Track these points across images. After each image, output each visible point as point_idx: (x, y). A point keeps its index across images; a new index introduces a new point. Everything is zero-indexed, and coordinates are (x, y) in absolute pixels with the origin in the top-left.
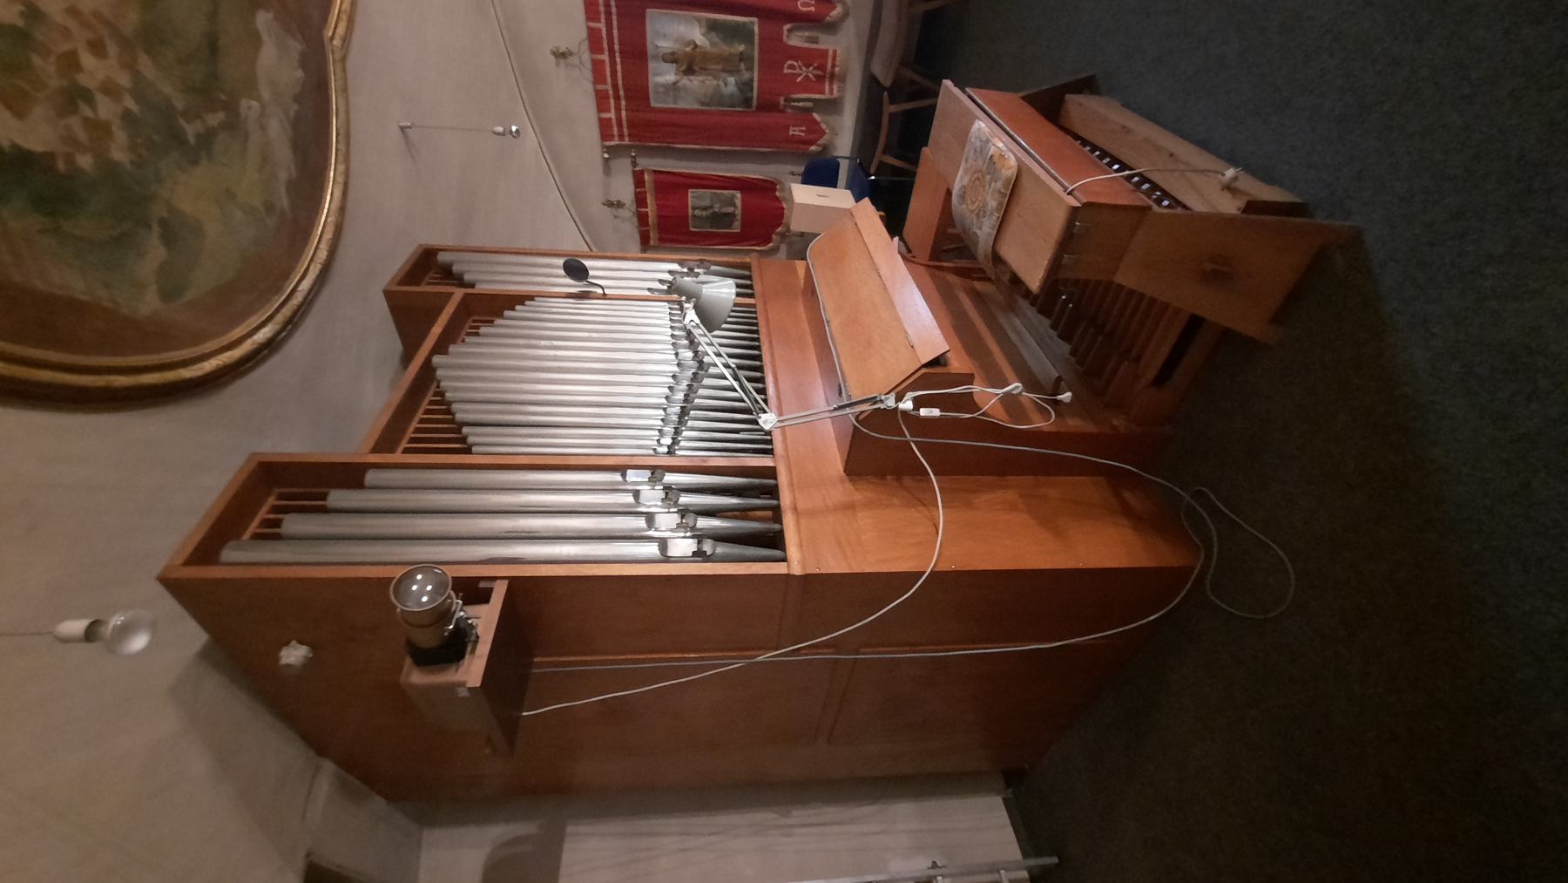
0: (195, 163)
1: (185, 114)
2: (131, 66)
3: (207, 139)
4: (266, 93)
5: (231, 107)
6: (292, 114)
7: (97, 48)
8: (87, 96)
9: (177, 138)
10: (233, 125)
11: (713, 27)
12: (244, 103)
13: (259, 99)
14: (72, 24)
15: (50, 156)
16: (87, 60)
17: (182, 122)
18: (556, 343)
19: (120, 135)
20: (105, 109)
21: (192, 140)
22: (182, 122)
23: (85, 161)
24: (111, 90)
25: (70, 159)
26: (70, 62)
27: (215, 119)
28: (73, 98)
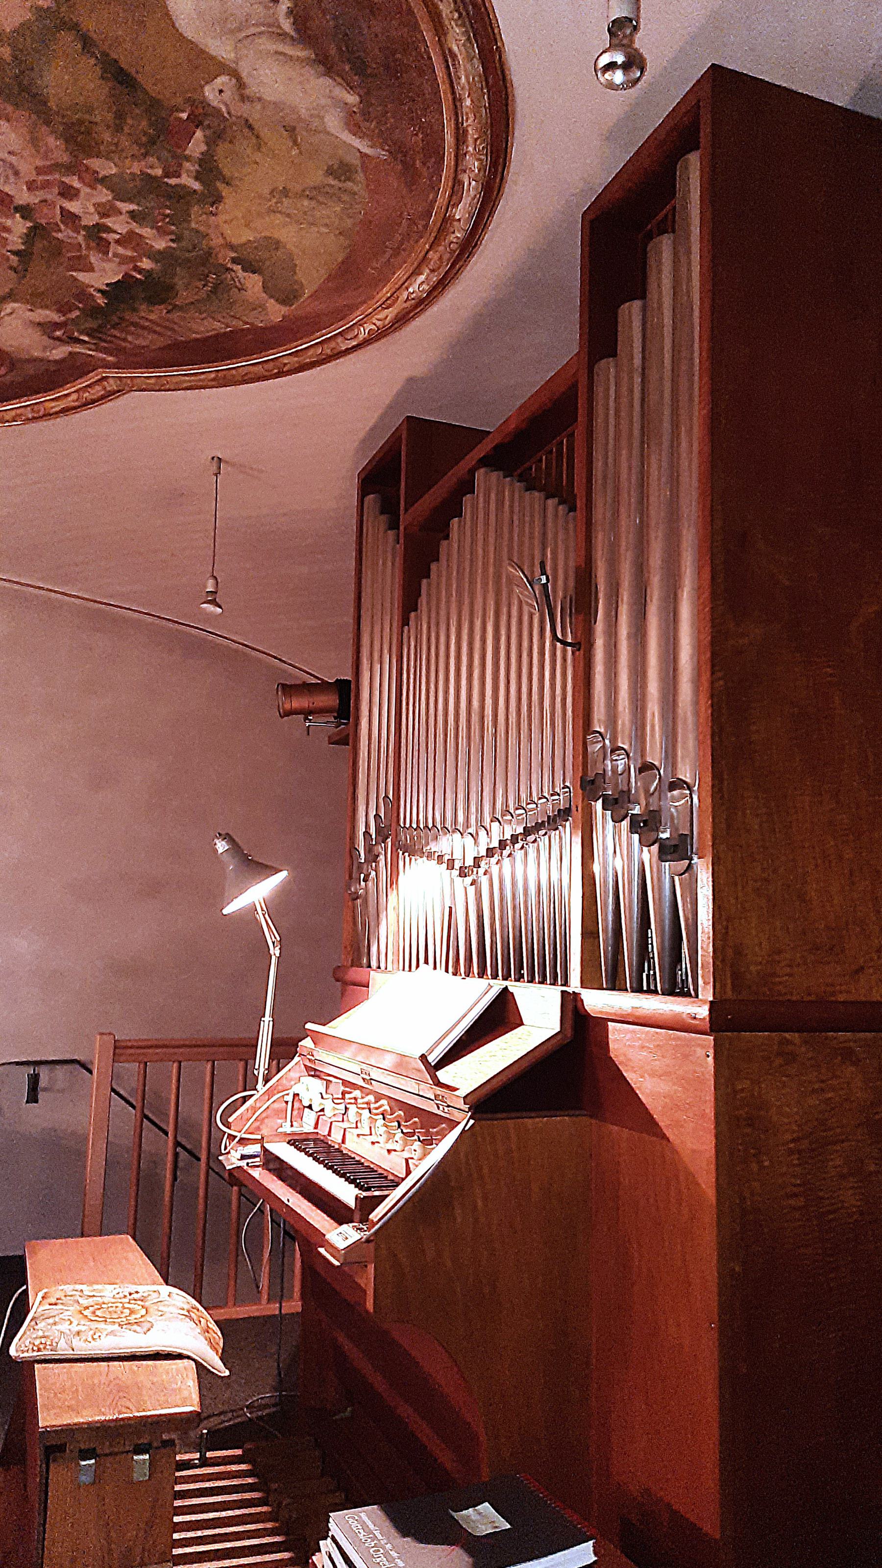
0: (218, 199)
1: (167, 175)
2: (96, 180)
3: (208, 170)
4: (220, 48)
5: (202, 114)
6: (287, 25)
7: (68, 193)
8: (101, 228)
9: (181, 195)
10: (220, 127)
11: (453, 1115)
12: (210, 93)
13: (222, 68)
14: (41, 195)
15: (127, 275)
16: (73, 207)
17: (173, 181)
18: (503, 632)
19: (146, 232)
20: (120, 225)
21: (196, 186)
22: (173, 181)
23: (146, 264)
24: (106, 211)
25: (140, 271)
26: (70, 218)
27: (197, 145)
28: (97, 235)
